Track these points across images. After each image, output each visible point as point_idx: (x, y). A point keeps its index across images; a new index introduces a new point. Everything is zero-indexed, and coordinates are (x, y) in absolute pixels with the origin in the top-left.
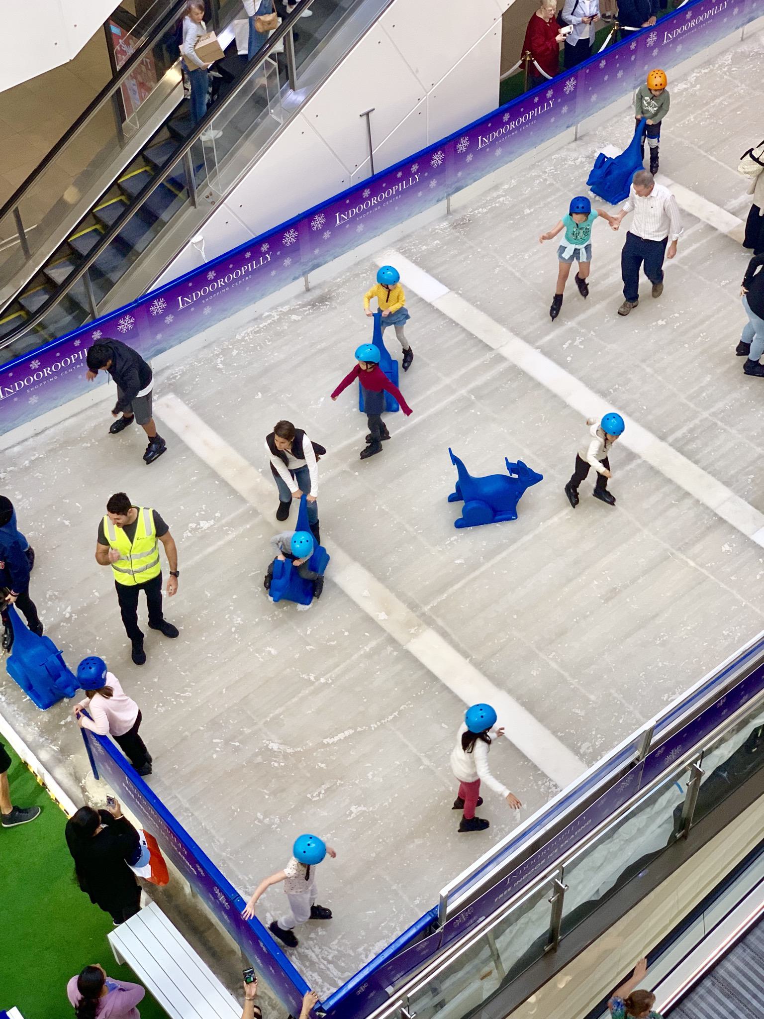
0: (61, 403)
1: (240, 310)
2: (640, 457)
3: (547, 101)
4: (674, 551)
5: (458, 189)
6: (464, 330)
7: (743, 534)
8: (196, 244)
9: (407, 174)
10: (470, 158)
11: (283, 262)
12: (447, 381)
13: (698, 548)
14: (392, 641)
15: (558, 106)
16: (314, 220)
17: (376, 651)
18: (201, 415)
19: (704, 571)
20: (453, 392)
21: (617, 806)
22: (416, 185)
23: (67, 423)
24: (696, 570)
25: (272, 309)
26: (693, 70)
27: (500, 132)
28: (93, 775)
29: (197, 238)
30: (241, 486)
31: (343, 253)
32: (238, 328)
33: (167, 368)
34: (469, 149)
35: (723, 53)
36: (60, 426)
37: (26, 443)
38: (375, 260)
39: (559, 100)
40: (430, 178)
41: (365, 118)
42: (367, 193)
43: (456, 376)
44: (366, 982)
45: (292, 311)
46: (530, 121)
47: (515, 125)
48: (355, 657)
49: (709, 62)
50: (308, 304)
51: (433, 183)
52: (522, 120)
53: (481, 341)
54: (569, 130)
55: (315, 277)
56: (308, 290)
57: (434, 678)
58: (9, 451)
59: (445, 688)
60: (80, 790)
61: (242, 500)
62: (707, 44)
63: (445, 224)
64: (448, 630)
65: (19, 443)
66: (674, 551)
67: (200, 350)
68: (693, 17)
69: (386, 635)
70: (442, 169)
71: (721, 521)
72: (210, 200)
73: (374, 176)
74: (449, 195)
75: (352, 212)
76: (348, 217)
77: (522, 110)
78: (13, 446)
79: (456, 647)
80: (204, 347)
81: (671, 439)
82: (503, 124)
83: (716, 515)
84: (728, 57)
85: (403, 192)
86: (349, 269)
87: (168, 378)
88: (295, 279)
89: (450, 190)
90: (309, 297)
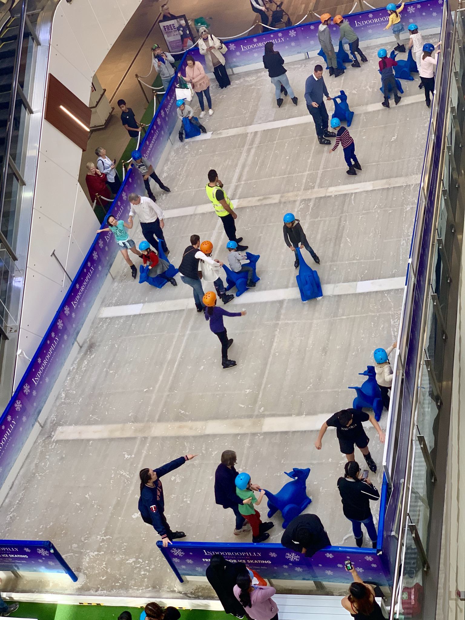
0: (12, 465)
1: (16, 459)
2: (285, 300)
3: (54, 339)
4: (333, 319)
5: (78, 333)
6: (164, 312)
7: (352, 294)
8: (20, 354)
9: (52, 340)
10: (34, 393)
11: (22, 420)
12: (177, 334)
13: (340, 311)
14: (254, 434)
15: (61, 338)
16: (24, 389)
17: (252, 442)
18: (82, 424)
19: (351, 316)
20: (184, 336)
21: (409, 420)
22: (94, 272)
23: (21, 473)
24: (348, 318)
25: (72, 365)
26: (163, 167)
27: (84, 285)
28: (178, 580)
29: (19, 352)
30: (128, 434)
31: (85, 320)
32: (64, 382)
33: (47, 419)
34: (31, 389)
35: (169, 153)
36: (19, 477)
37: (9, 495)
38: (99, 317)
39: (60, 335)
40: (21, 418)
41: (53, 256)
42: (39, 360)
43: (179, 329)
44: (450, 11)
45: (82, 359)
46: (52, 354)
47: (46, 361)
48: (245, 452)
49: (167, 160)
50: (87, 351)
51: (24, 419)
52: (48, 356)
53: (176, 311)
54: (35, 427)
55: (81, 338)
56: (81, 347)
57: (286, 433)
58: (4, 503)
59: (294, 432)
60: (179, 594)
61: (135, 438)
62: (161, 152)
63: (116, 284)
64: (274, 413)
65: (6, 498)
66: (333, 319)
67: (55, 403)
68: (150, 143)
69: (249, 435)
70: (24, 409)
71: (339, 296)
72: (13, 331)
73: (73, 282)
74: (109, 270)
75: (39, 374)
76: (38, 378)
77: (45, 352)
78: (4, 501)
79: (283, 415)
80: (56, 400)
81: (290, 285)
82: (78, 291)
83: (335, 296)
84: (173, 153)
85: (11, 434)
86: (91, 327)
87: (51, 423)
88: (33, 425)
89: (108, 268)
90: (84, 349)
